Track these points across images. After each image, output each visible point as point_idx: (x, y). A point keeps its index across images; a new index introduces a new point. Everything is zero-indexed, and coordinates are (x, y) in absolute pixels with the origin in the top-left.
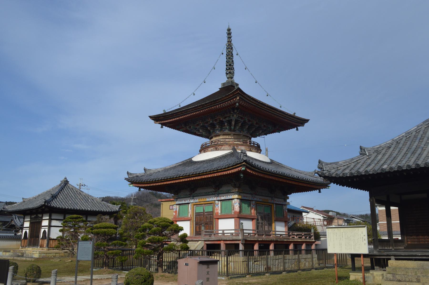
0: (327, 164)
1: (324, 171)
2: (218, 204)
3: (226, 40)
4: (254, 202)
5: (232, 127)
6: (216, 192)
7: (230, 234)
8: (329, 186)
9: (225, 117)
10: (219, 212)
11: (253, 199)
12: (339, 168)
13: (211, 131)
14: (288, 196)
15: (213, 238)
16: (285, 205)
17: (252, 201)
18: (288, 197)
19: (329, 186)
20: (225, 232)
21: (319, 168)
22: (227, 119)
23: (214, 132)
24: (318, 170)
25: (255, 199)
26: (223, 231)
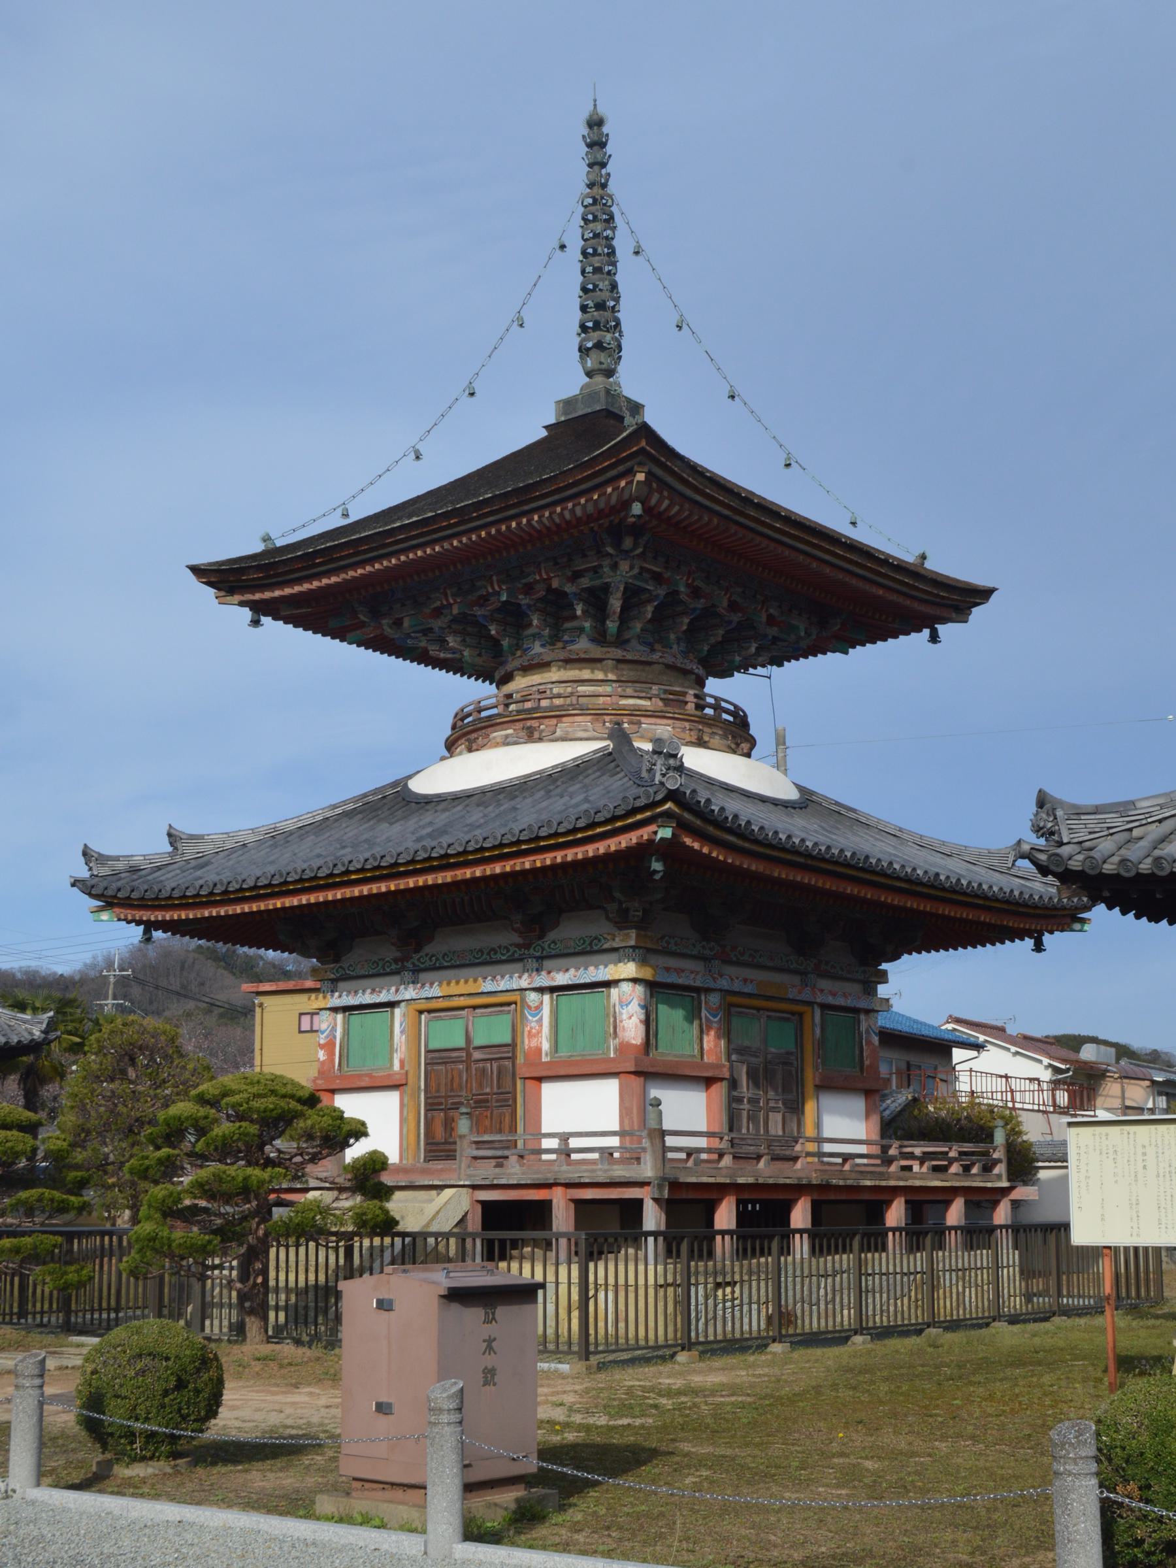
0: (1078, 812)
1: (1061, 844)
2: (539, 1008)
3: (580, 173)
4: (714, 999)
5: (612, 626)
8: (1083, 921)
9: (576, 576)
10: (546, 1046)
11: (712, 985)
12: (1136, 833)
13: (505, 643)
14: (884, 966)
15: (514, 1172)
17: (708, 990)
18: (885, 973)
19: (1083, 921)
20: (574, 1143)
21: (1038, 830)
22: (585, 582)
23: (518, 647)
24: (1033, 840)
25: (724, 983)
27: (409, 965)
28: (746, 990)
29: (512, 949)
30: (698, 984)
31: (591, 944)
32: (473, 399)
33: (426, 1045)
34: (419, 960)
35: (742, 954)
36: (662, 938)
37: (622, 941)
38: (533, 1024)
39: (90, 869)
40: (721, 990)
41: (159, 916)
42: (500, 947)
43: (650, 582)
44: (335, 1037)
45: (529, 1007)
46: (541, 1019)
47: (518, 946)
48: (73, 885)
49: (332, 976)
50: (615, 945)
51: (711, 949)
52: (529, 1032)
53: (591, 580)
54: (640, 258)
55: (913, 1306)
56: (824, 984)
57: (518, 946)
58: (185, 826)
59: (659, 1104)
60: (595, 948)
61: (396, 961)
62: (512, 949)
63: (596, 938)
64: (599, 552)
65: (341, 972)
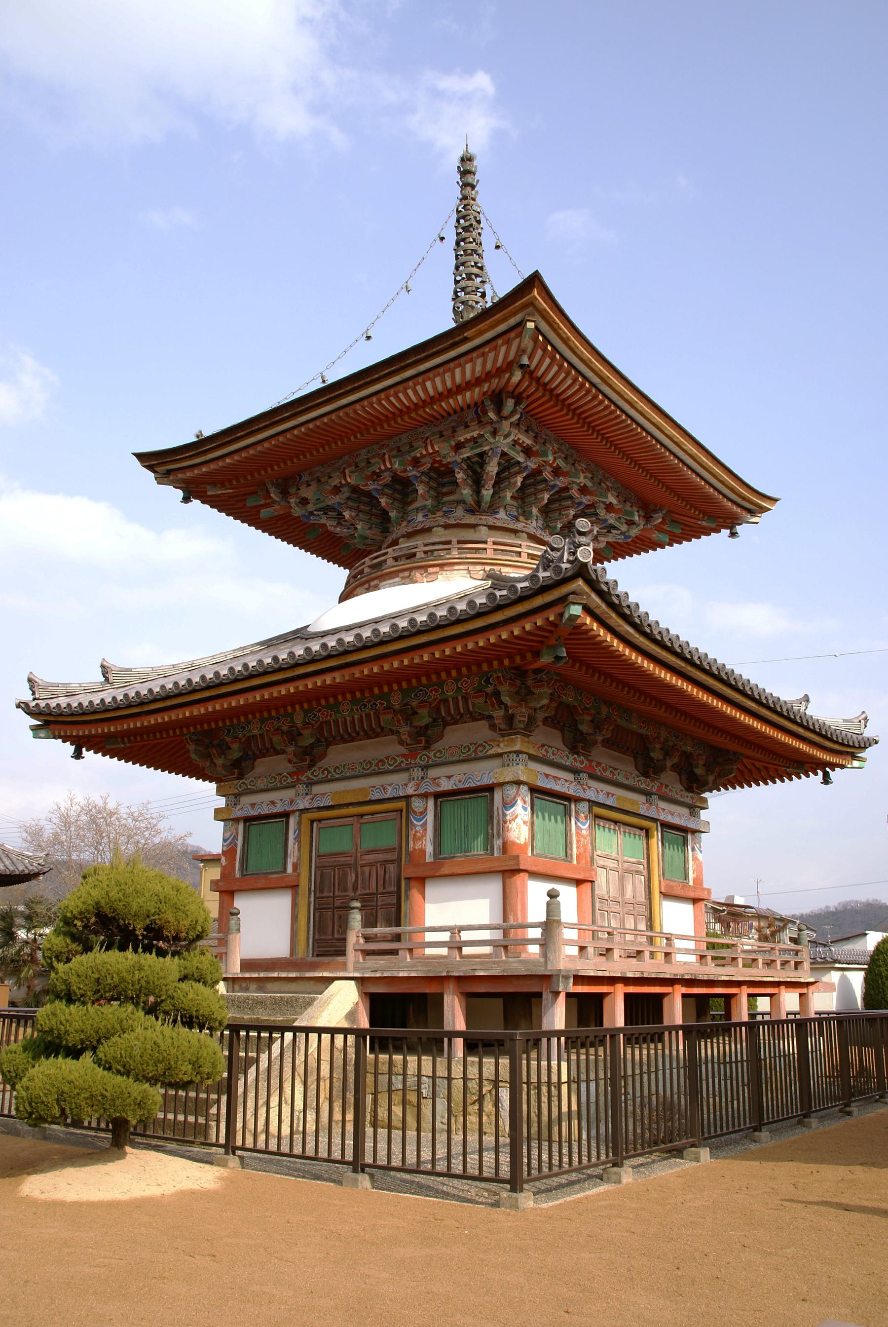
2: (423, 813)
3: (456, 192)
4: (584, 806)
5: (487, 493)
6: (413, 755)
7: (487, 950)
9: (459, 447)
10: (429, 849)
11: (582, 795)
13: (393, 514)
14: (706, 795)
15: (403, 967)
16: (694, 832)
17: (578, 800)
18: (705, 800)
20: (465, 936)
22: (466, 453)
23: (403, 519)
25: (591, 795)
26: (455, 930)
27: (304, 778)
28: (608, 803)
29: (399, 760)
30: (571, 792)
31: (475, 751)
32: (371, 341)
33: (317, 850)
34: (312, 774)
35: (605, 771)
36: (543, 746)
37: (507, 746)
38: (418, 828)
39: (34, 693)
40: (589, 801)
41: (86, 731)
42: (387, 758)
43: (521, 454)
44: (236, 845)
45: (414, 812)
46: (425, 823)
47: (403, 756)
48: (18, 706)
49: (236, 791)
50: (500, 751)
51: (582, 763)
52: (414, 835)
53: (472, 449)
54: (500, 250)
55: (630, 1090)
56: (662, 804)
57: (403, 756)
58: (117, 661)
59: (558, 896)
60: (481, 754)
61: (291, 775)
62: (399, 760)
63: (480, 745)
64: (480, 422)
65: (243, 786)
